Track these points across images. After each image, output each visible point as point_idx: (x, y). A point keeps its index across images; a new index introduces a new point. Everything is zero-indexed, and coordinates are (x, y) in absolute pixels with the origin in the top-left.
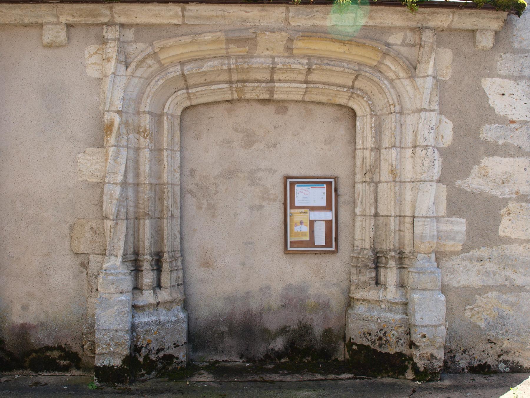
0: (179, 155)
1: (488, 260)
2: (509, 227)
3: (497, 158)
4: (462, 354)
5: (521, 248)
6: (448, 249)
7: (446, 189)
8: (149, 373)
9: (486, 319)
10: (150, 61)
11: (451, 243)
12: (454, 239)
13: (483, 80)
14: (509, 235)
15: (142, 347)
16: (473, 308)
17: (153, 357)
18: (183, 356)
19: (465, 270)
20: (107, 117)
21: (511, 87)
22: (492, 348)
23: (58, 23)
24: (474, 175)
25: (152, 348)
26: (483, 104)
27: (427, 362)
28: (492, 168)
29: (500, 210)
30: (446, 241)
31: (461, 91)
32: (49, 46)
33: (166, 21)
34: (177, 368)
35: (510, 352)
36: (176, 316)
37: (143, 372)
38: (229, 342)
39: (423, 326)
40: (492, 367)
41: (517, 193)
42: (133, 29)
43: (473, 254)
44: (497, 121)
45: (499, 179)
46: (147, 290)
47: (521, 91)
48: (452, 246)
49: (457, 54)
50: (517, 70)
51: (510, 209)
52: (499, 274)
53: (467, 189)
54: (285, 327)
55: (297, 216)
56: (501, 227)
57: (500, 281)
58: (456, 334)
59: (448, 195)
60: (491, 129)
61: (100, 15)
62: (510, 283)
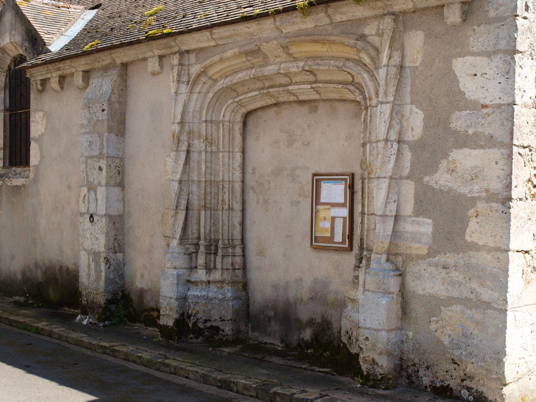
0: (239, 156)
1: (454, 268)
2: (476, 231)
3: (466, 151)
4: (425, 370)
5: (489, 257)
6: (414, 252)
7: (414, 187)
8: (197, 338)
9: (450, 336)
10: (203, 79)
11: (417, 245)
12: (419, 242)
13: (454, 61)
14: (476, 240)
15: (191, 315)
16: (438, 321)
17: (201, 326)
18: (229, 331)
19: (431, 276)
21: (484, 66)
22: (455, 369)
24: (442, 170)
25: (199, 318)
26: (453, 88)
27: (369, 366)
28: (461, 162)
29: (468, 210)
30: (411, 243)
31: (431, 76)
32: (153, 74)
33: (207, 45)
34: (223, 339)
35: (473, 378)
36: (223, 294)
37: (192, 336)
38: (275, 327)
39: (365, 328)
40: (455, 392)
41: (487, 190)
42: (194, 53)
43: (438, 260)
44: (468, 106)
45: (467, 175)
46: (201, 269)
47: (495, 69)
48: (418, 248)
49: (428, 36)
50: (491, 43)
51: (478, 210)
52: (465, 285)
54: (312, 320)
55: (324, 213)
57: (466, 294)
58: (420, 346)
59: (415, 193)
60: (461, 117)
62: (476, 297)
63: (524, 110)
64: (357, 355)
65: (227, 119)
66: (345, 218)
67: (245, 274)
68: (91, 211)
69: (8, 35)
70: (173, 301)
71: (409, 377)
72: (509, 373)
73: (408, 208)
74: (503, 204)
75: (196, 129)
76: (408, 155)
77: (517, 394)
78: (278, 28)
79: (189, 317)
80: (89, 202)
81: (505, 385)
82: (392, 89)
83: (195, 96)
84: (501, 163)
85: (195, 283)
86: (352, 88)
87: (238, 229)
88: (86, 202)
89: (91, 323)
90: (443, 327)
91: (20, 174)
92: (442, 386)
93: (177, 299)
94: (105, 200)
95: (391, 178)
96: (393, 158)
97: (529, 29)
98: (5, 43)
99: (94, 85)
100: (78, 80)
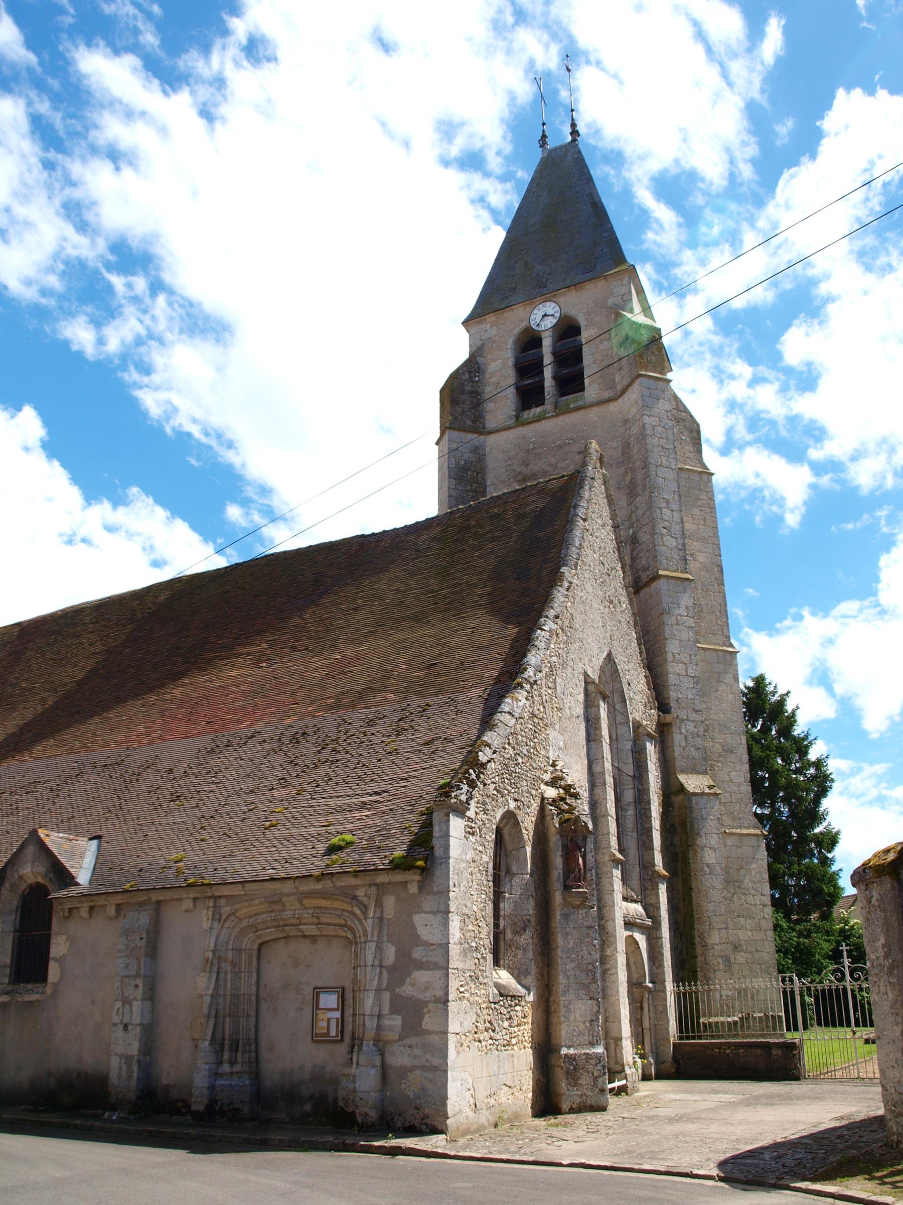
3: (422, 972)
5: (436, 1038)
6: (390, 1038)
10: (232, 918)
11: (392, 1033)
12: (393, 1031)
17: (225, 1108)
20: (207, 954)
23: (189, 898)
32: (186, 911)
33: (237, 893)
49: (397, 899)
53: (403, 994)
55: (321, 1015)
56: (424, 1023)
61: (207, 892)
63: (454, 946)
64: (353, 1113)
65: (248, 948)
66: (338, 1019)
67: (257, 1066)
68: (125, 1021)
69: (29, 865)
70: (204, 1089)
71: (387, 1123)
72: (450, 1112)
73: (386, 1009)
74: (444, 1004)
75: (223, 955)
76: (385, 975)
77: (454, 1125)
78: (295, 887)
79: (216, 1102)
80: (123, 1014)
81: (448, 1118)
82: (376, 933)
83: (224, 930)
84: (443, 979)
85: (221, 1075)
86: (346, 929)
87: (253, 1030)
88: (120, 1013)
89: (121, 1117)
90: (409, 1086)
91: (33, 990)
92: (410, 1126)
93: (208, 1088)
94: (140, 1012)
95: (376, 990)
96: (377, 977)
97: (456, 898)
98: (25, 871)
99: (130, 917)
100: (112, 911)
